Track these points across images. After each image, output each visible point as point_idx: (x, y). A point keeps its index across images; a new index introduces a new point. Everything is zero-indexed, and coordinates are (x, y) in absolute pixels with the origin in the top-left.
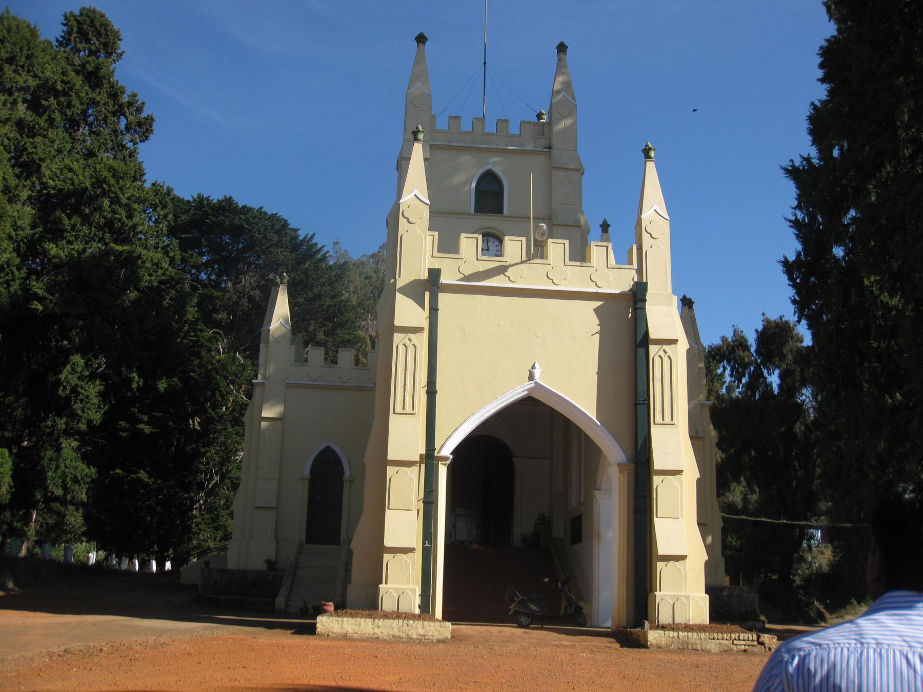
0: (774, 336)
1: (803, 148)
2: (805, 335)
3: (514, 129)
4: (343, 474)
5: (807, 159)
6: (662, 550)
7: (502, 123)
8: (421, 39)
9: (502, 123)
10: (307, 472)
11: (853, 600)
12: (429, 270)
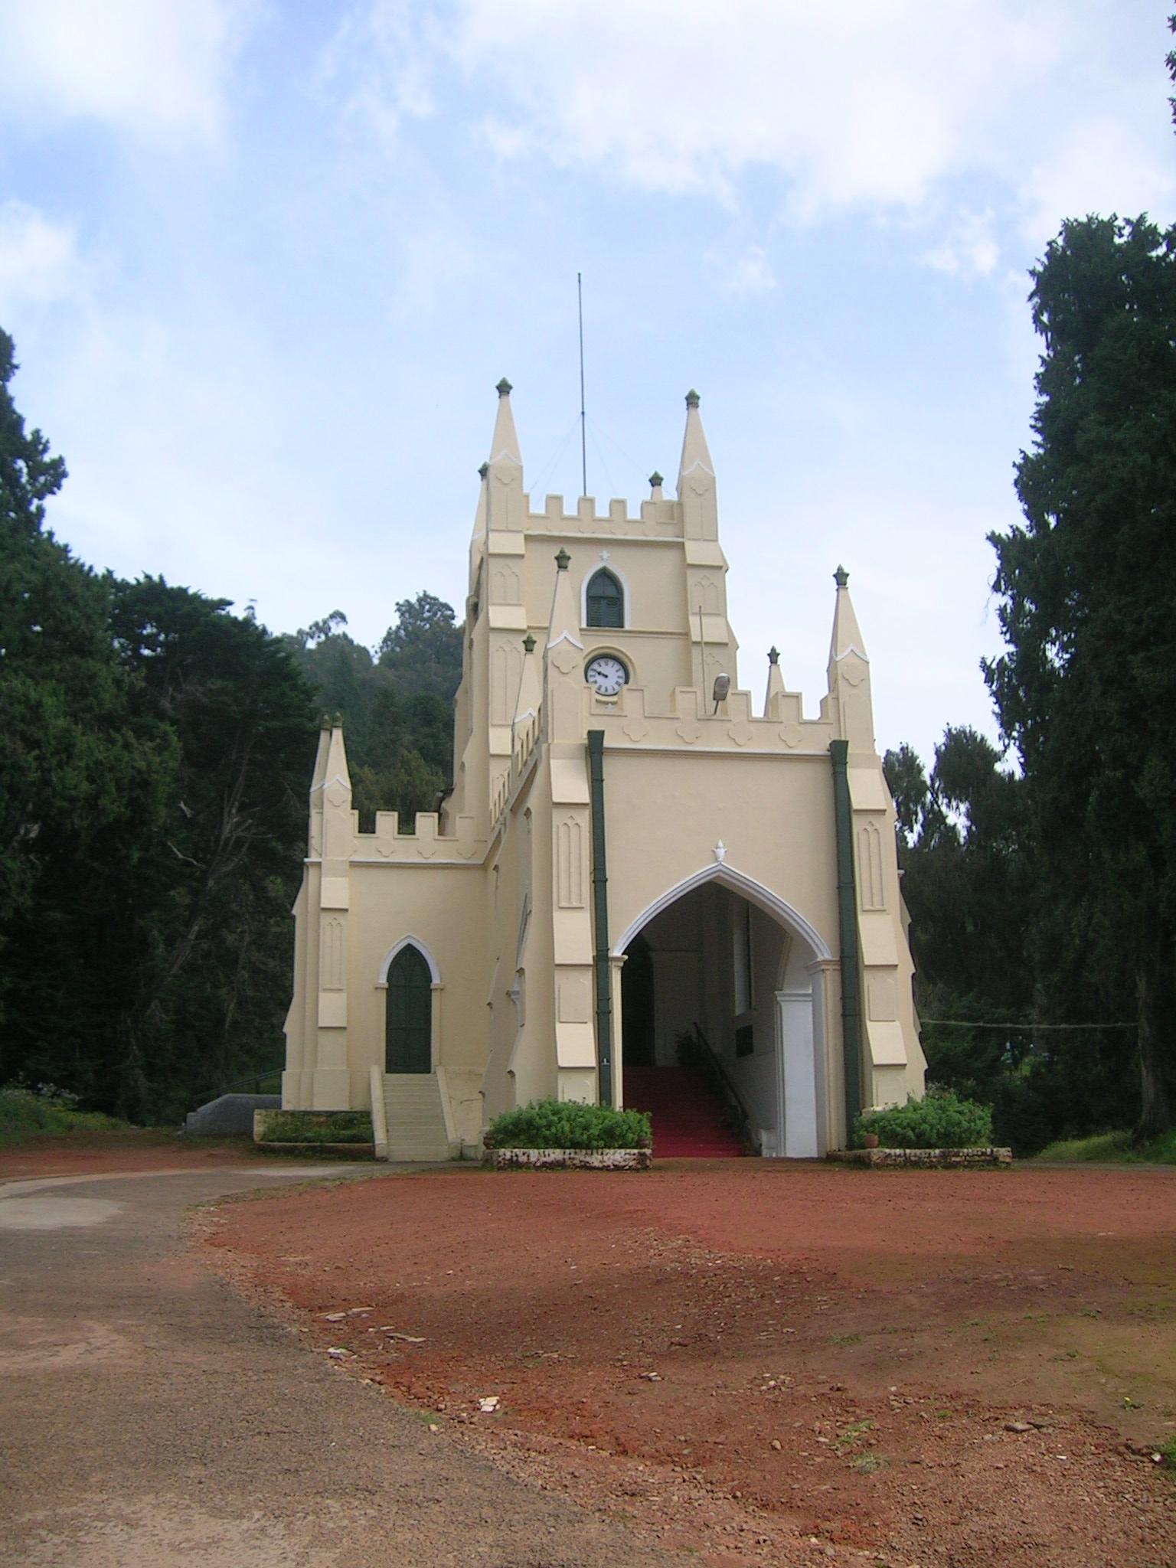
0: (963, 757)
1: (1010, 515)
2: (1011, 764)
3: (633, 514)
4: (429, 979)
5: (1015, 530)
6: (878, 1058)
7: (618, 505)
8: (504, 388)
9: (618, 505)
10: (383, 981)
11: (1045, 399)
12: (589, 732)
